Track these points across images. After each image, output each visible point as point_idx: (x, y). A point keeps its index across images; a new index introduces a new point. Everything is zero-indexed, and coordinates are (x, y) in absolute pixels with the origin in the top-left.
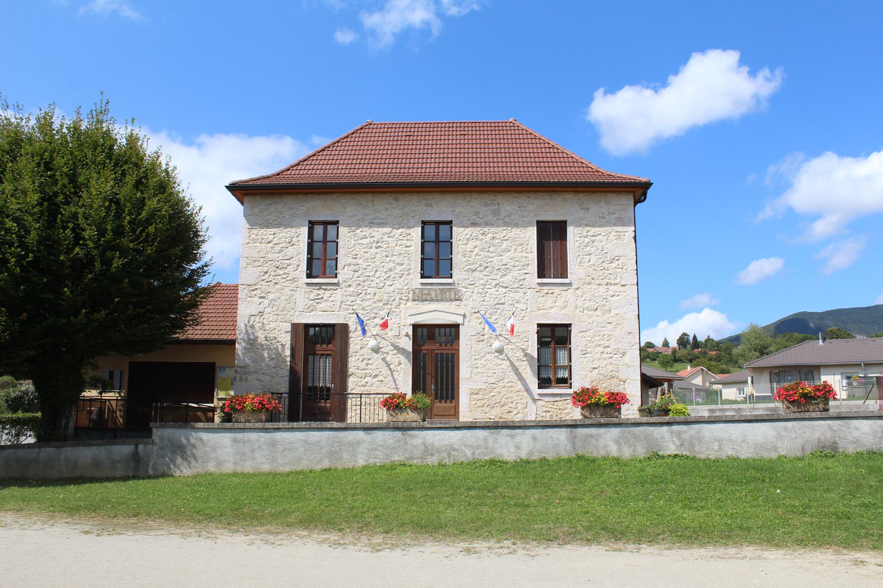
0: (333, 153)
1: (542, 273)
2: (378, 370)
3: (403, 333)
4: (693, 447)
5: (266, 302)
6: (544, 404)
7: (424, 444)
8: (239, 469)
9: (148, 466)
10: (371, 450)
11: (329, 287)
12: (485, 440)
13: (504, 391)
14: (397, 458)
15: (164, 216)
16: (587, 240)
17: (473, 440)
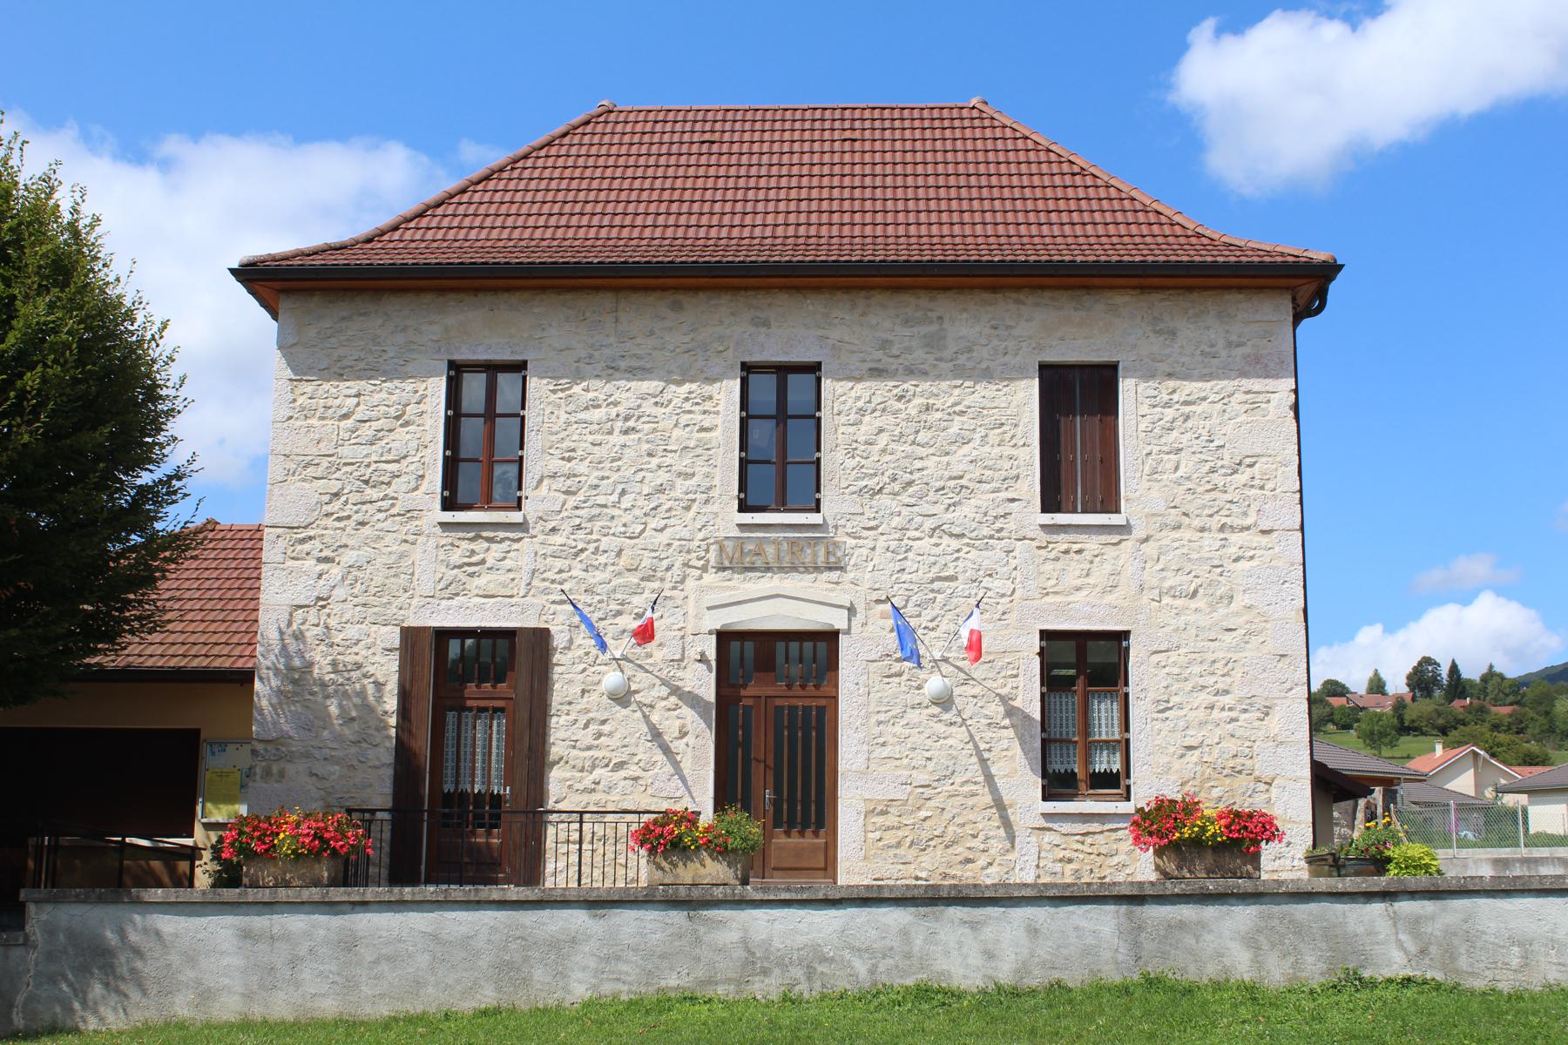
0: (512, 185)
2: (625, 748)
3: (693, 653)
4: (1453, 958)
5: (336, 571)
7: (745, 943)
8: (257, 1012)
9: (11, 1006)
10: (607, 959)
11: (502, 534)
12: (905, 933)
14: (673, 982)
15: (67, 346)
16: (1170, 413)
17: (873, 934)
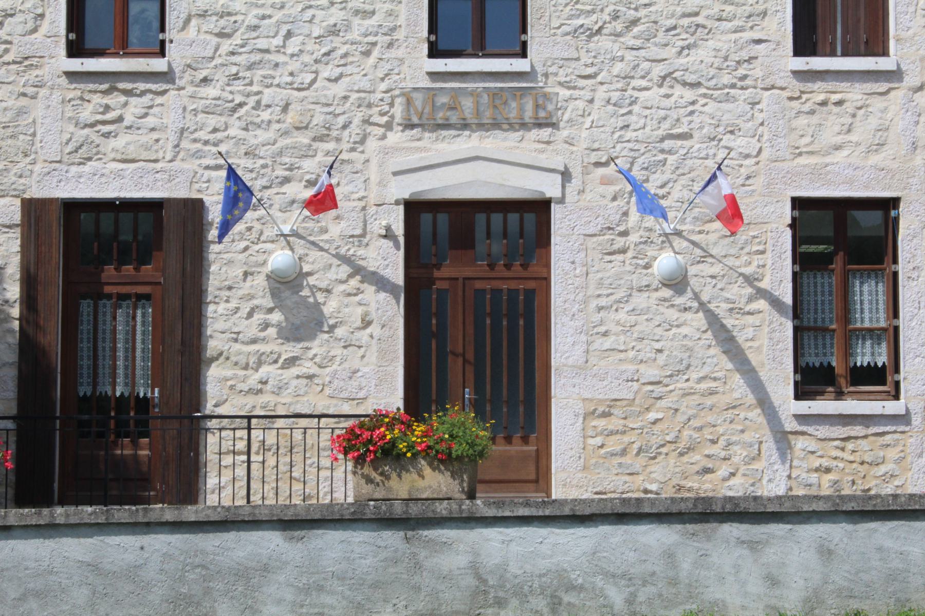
1: (806, 41)
3: (377, 227)
6: (812, 445)
7: (475, 569)
10: (306, 590)
11: (142, 86)
12: (670, 556)
13: (688, 406)
17: (631, 556)
